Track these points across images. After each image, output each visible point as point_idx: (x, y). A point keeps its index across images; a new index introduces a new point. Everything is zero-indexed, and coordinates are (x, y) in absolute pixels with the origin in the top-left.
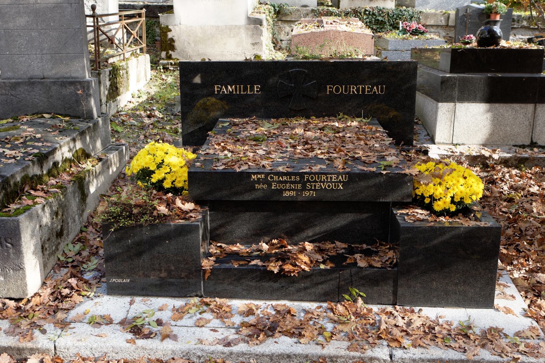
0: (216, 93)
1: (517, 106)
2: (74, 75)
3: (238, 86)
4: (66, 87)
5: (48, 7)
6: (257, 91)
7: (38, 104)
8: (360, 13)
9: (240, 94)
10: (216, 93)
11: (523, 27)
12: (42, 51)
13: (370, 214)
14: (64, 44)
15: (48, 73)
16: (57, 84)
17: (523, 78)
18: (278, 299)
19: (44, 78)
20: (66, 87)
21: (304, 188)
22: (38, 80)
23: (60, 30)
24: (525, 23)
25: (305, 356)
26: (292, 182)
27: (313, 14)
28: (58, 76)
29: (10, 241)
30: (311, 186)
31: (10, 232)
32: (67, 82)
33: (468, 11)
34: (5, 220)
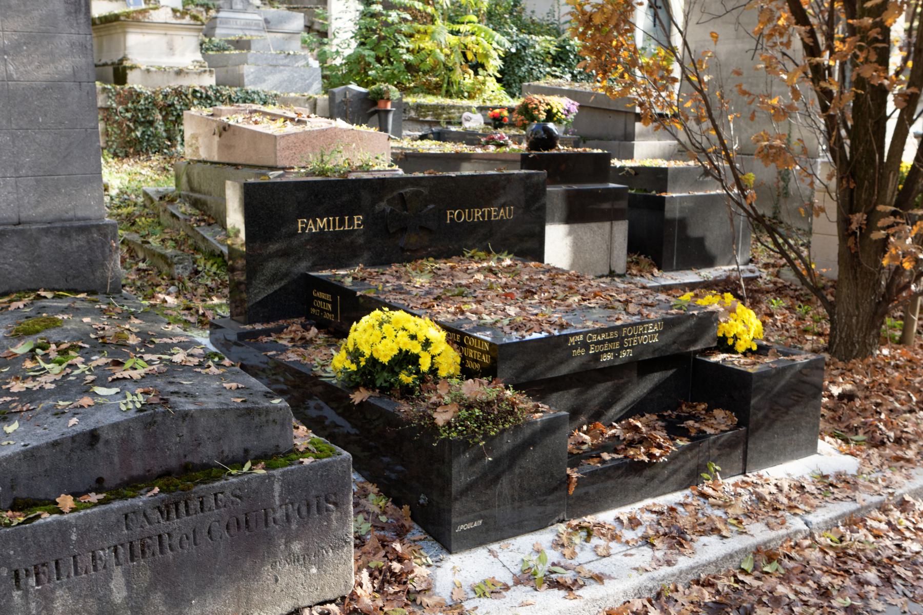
0: (300, 232)
1: (594, 226)
2: (80, 214)
3: (331, 219)
4: (69, 237)
5: (33, 88)
6: (359, 225)
7: (10, 273)
8: (186, 96)
9: (335, 231)
10: (300, 232)
11: (412, 120)
12: (16, 170)
13: (674, 370)
14: (64, 157)
15: (28, 213)
16: (52, 232)
17: (598, 189)
18: (641, 500)
19: (19, 224)
20: (69, 237)
21: (622, 347)
22: (10, 227)
23: (57, 131)
24: (413, 114)
25: (753, 550)
26: (610, 341)
27: (105, 95)
28: (50, 217)
29: (333, 498)
30: (628, 342)
31: (335, 483)
32: (72, 227)
33: (348, 96)
34: (329, 462)
